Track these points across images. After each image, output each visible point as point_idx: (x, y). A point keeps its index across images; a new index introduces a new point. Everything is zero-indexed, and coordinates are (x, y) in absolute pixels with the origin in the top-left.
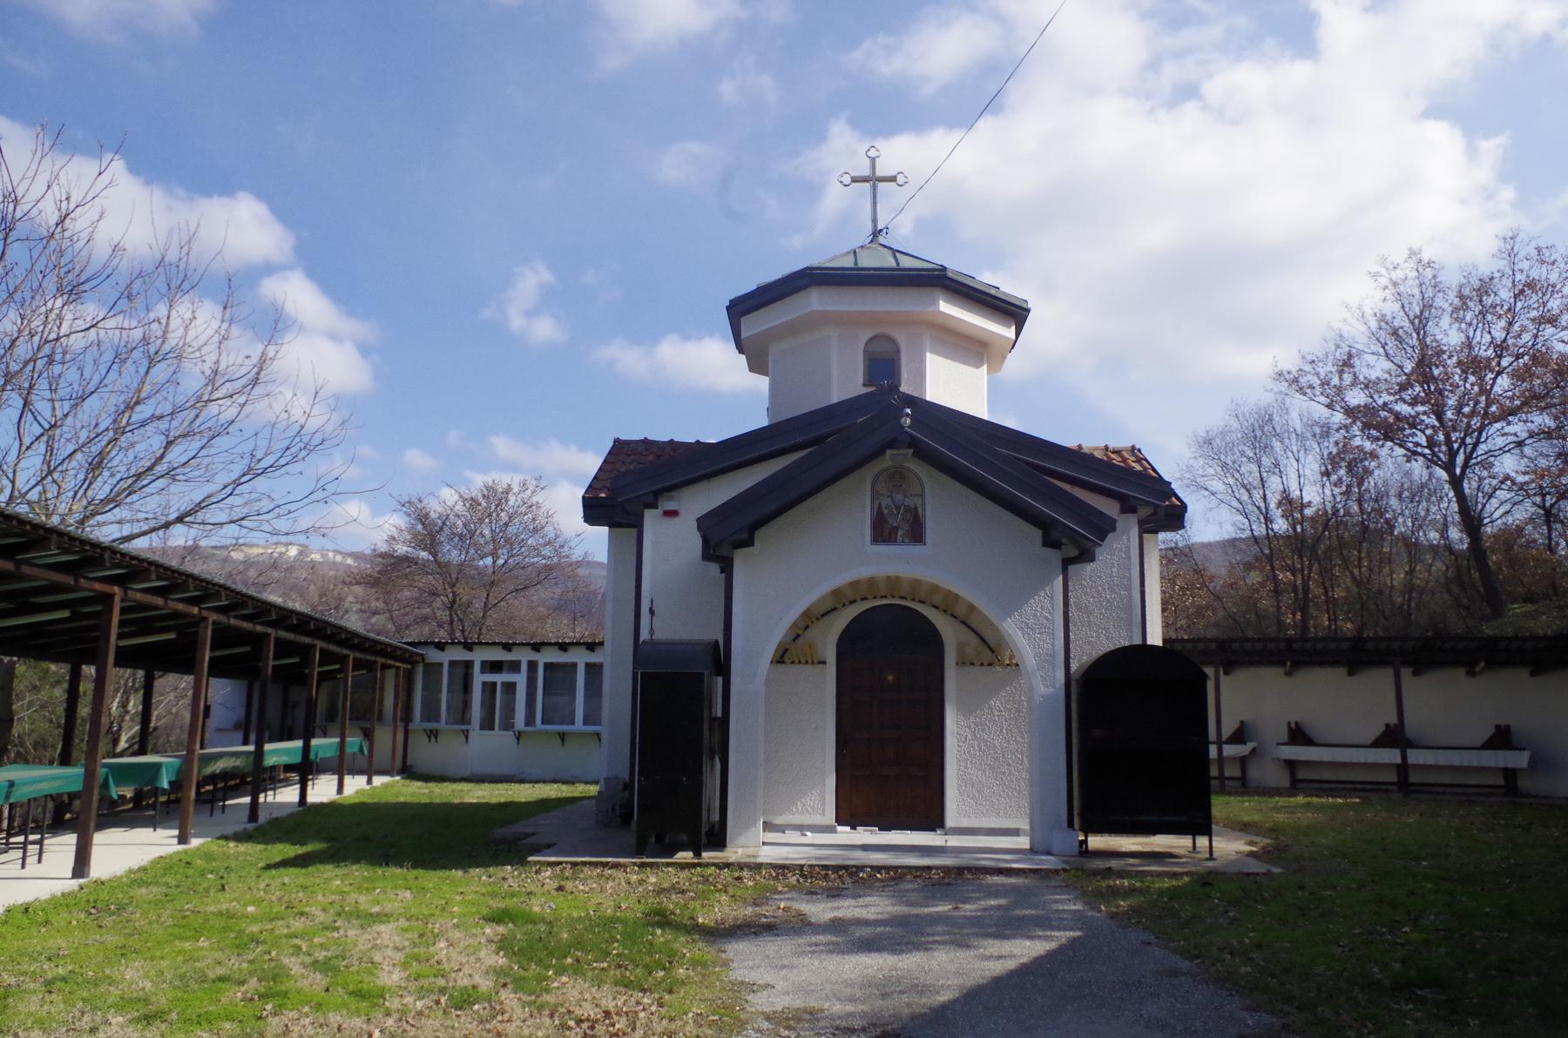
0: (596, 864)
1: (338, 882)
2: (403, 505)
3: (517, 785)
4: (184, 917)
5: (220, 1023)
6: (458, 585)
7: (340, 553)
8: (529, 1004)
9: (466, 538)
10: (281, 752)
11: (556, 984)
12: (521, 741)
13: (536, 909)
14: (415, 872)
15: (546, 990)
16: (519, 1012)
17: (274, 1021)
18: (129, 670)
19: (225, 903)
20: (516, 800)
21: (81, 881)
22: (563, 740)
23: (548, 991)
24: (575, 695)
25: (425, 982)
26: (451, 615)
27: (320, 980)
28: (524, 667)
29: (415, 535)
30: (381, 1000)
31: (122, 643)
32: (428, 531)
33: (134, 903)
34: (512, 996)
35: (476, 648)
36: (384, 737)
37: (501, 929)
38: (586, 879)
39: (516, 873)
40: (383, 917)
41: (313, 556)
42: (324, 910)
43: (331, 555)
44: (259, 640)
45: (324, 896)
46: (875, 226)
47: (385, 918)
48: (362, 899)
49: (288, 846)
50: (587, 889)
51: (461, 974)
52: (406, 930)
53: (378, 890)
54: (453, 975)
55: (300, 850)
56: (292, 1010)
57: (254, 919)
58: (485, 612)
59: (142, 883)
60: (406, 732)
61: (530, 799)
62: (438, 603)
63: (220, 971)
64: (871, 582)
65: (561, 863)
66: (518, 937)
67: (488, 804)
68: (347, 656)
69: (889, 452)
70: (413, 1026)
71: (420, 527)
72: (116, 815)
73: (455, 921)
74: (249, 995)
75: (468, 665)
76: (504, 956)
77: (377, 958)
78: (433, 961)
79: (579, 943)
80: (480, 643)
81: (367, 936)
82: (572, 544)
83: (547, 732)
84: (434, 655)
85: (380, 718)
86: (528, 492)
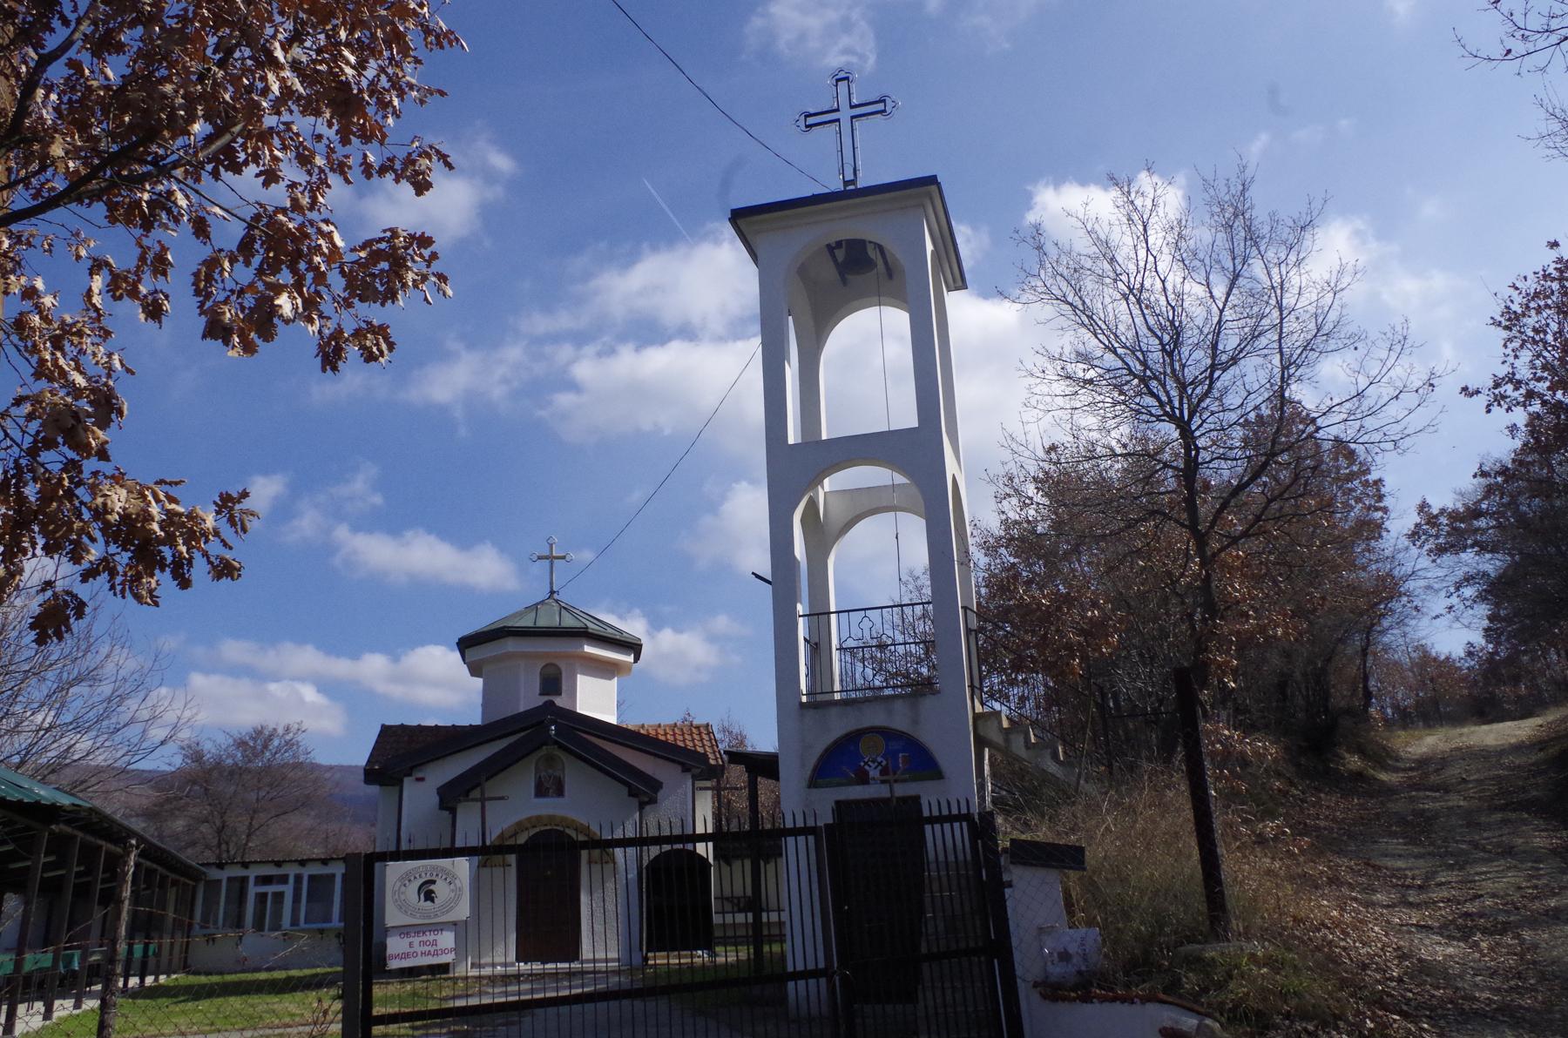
28: (291, 880)
31: (77, 881)
35: (252, 867)
46: (552, 587)
64: (539, 818)
69: (544, 747)
75: (244, 880)
84: (214, 874)
86: (291, 735)
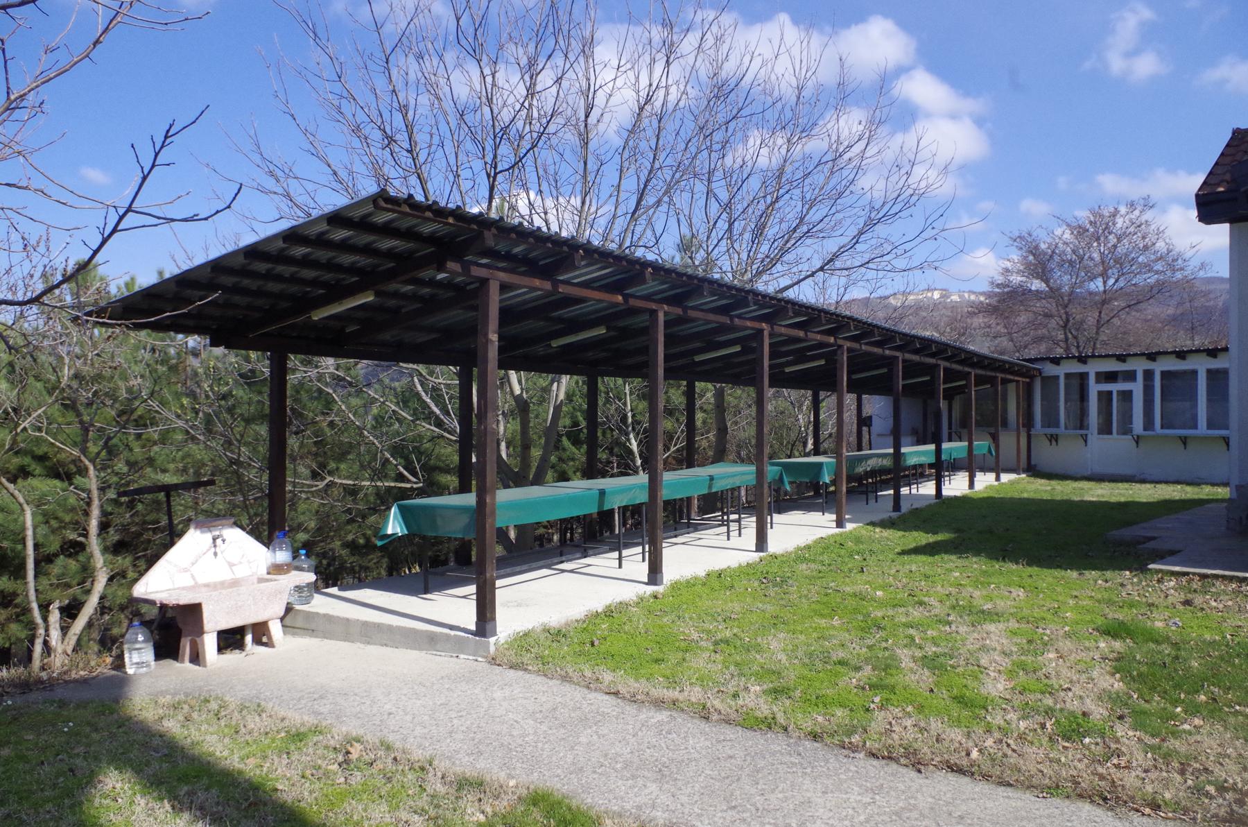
0: (1231, 579)
1: (958, 574)
2: (1015, 240)
3: (1138, 485)
4: (826, 595)
5: (834, 708)
6: (1070, 306)
7: (974, 293)
8: (1152, 748)
9: (1076, 263)
10: (917, 453)
11: (1186, 727)
12: (1140, 444)
13: (1159, 624)
14: (1029, 570)
15: (1173, 733)
16: (1140, 758)
17: (880, 715)
18: (565, 379)
19: (859, 584)
20: (1137, 500)
21: (762, 554)
22: (1185, 444)
23: (1176, 735)
24: (1196, 400)
25: (1031, 697)
26: (1065, 334)
27: (926, 677)
29: (1028, 265)
30: (983, 712)
32: (1039, 263)
33: (795, 577)
34: (1131, 733)
36: (1008, 441)
37: (1118, 645)
38: (1218, 594)
39: (1135, 580)
40: (993, 616)
41: (953, 297)
42: (941, 602)
43: (966, 295)
44: (890, 362)
45: (943, 586)
47: (995, 617)
48: (977, 594)
49: (922, 534)
50: (1221, 606)
51: (1070, 694)
52: (1015, 634)
53: (993, 586)
54: (1062, 694)
55: (931, 538)
56: (897, 707)
57: (881, 604)
58: (1098, 329)
59: (803, 560)
60: (1029, 437)
61: (1151, 500)
62: (1053, 323)
63: (841, 654)
65: (1187, 574)
66: (1138, 657)
67: (1107, 503)
68: (970, 373)
70: (1014, 751)
71: (1031, 258)
72: (783, 505)
73: (1067, 628)
74: (862, 684)
75: (1083, 377)
76: (1121, 680)
77: (983, 662)
78: (1040, 674)
79: (1213, 676)
80: (1093, 356)
81: (976, 635)
82: (1187, 256)
83: (1166, 436)
84: (1050, 369)
85: (1005, 424)
